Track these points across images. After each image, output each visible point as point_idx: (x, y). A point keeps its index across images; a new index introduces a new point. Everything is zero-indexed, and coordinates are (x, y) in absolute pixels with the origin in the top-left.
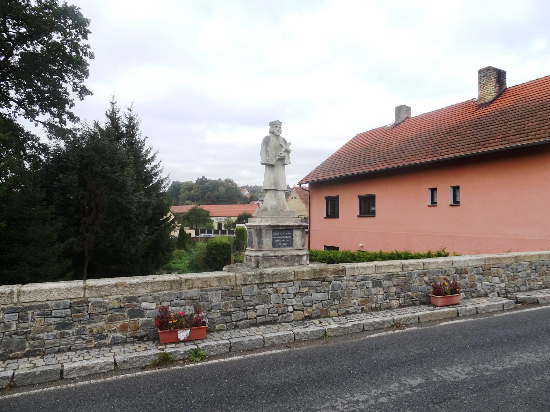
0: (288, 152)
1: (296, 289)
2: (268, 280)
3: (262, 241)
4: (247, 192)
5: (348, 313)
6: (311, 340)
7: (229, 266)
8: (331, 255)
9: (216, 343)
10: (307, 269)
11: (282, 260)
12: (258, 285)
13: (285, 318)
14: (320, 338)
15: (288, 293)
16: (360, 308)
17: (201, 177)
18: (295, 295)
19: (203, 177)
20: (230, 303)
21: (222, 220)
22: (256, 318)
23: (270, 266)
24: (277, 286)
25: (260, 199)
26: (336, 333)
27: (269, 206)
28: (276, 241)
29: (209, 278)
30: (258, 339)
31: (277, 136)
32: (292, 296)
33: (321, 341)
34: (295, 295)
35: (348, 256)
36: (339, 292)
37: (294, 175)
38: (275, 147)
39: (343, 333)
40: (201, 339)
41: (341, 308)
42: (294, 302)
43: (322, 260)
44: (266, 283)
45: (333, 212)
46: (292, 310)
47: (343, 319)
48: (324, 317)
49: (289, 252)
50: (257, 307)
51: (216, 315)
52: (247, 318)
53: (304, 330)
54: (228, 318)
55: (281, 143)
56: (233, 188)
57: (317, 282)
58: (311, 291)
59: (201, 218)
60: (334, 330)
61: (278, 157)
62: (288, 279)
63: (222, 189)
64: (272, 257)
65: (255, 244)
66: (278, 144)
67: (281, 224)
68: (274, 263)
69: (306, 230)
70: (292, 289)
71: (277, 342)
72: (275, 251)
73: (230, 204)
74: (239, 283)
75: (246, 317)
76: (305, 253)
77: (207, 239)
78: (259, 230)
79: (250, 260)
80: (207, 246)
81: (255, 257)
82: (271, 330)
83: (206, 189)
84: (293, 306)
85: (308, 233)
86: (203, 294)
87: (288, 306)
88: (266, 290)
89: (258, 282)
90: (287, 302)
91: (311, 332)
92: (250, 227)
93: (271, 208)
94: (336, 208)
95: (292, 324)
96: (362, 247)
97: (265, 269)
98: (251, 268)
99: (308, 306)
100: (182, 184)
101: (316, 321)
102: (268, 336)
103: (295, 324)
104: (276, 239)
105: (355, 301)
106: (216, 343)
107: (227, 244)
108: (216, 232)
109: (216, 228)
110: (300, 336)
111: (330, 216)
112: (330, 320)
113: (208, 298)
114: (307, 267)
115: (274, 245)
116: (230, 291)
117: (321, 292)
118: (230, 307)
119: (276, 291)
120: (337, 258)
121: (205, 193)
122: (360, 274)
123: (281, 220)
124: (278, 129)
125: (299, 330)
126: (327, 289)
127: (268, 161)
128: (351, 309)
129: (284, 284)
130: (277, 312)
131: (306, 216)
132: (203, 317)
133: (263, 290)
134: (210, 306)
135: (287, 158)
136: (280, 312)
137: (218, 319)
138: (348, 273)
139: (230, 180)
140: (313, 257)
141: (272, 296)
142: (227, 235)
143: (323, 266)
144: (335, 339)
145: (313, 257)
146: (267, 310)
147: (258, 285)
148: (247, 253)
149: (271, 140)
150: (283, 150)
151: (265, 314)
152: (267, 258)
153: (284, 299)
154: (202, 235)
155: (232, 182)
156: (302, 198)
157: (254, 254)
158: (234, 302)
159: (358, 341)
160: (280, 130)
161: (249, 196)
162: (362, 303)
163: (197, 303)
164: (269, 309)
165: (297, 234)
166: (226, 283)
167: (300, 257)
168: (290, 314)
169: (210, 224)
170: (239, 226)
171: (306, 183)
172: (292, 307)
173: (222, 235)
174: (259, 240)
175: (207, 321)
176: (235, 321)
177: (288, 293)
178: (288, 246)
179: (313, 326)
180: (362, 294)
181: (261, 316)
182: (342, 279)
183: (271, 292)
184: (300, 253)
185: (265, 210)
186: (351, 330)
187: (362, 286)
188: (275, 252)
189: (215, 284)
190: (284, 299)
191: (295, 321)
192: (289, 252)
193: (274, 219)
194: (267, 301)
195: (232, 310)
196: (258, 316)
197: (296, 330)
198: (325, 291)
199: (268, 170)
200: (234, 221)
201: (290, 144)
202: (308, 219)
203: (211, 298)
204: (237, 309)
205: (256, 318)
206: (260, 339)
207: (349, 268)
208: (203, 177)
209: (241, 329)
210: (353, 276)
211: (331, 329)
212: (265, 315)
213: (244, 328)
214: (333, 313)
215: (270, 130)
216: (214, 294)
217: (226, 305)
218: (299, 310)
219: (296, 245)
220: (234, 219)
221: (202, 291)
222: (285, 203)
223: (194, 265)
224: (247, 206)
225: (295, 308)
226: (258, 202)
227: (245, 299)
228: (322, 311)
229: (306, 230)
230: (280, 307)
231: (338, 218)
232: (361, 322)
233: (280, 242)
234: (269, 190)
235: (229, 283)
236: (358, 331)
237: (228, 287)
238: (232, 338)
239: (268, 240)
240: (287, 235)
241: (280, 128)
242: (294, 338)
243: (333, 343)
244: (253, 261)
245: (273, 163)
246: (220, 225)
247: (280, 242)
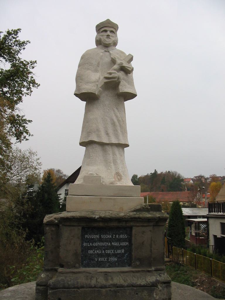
100: (183, 180)
135: (123, 83)
233: (101, 255)
240: (119, 240)
247: (101, 255)
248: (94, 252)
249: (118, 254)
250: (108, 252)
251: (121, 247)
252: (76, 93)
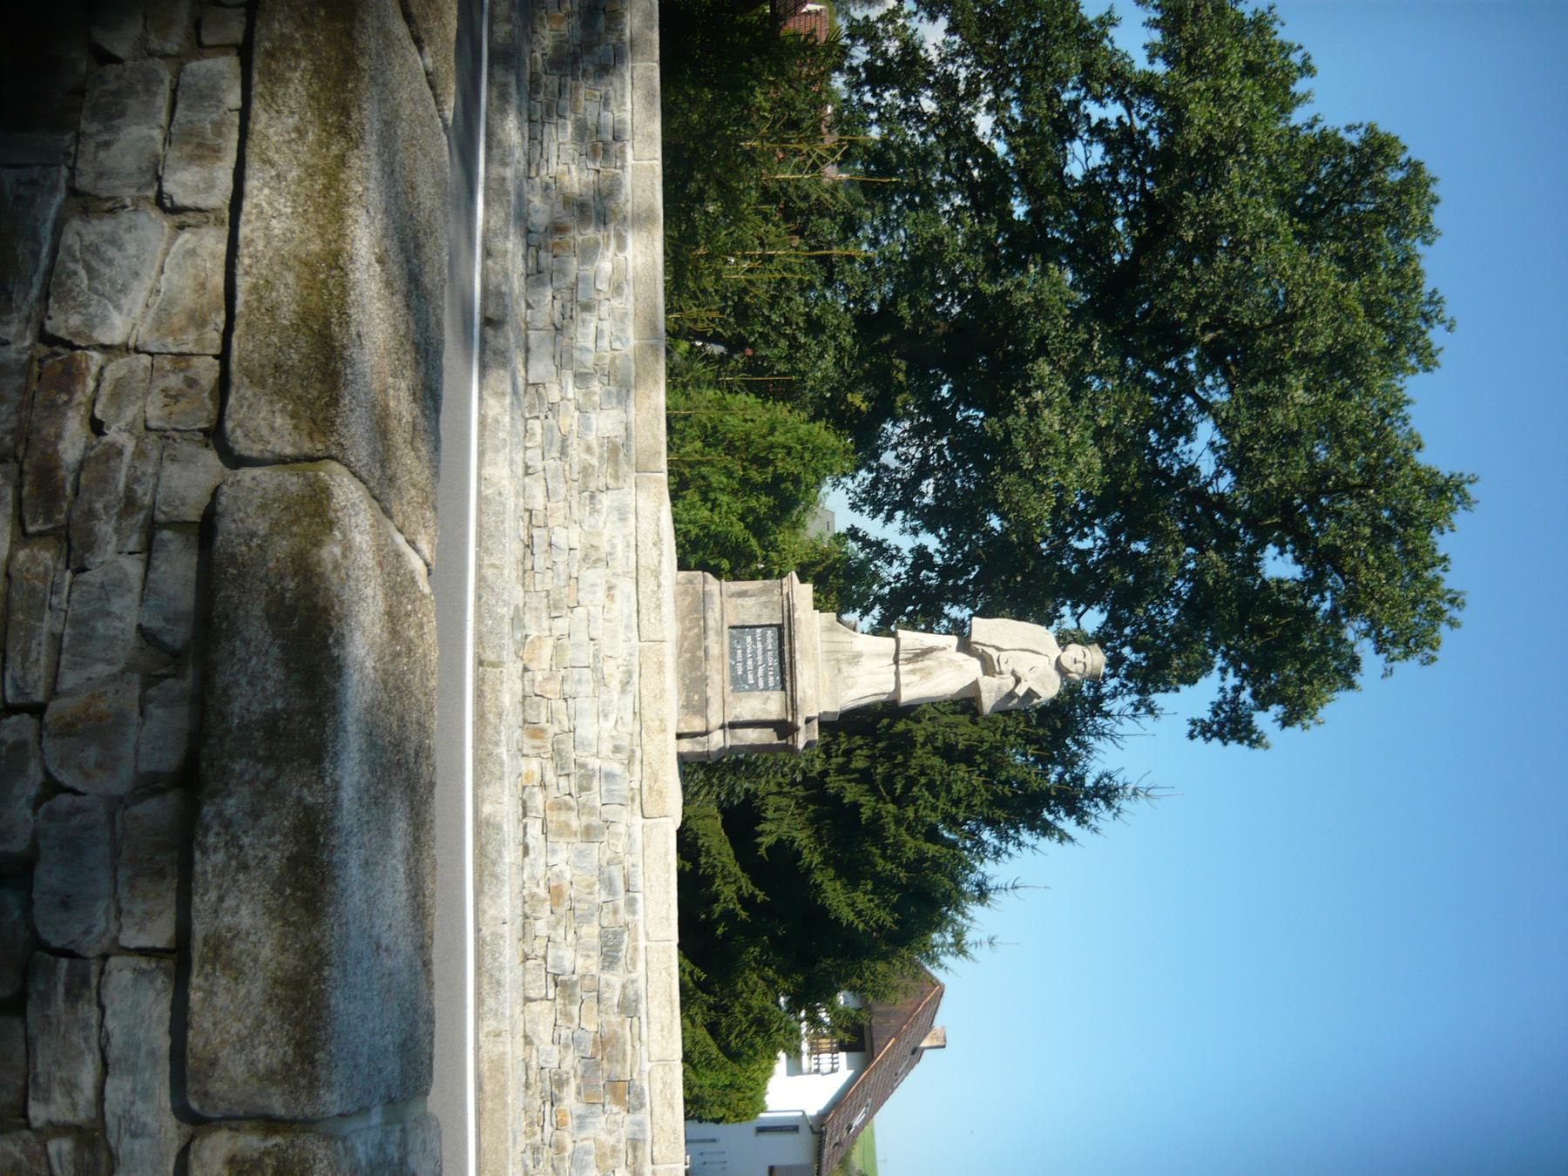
72: (720, 633)
233: (744, 653)
240: (765, 676)
247: (744, 653)
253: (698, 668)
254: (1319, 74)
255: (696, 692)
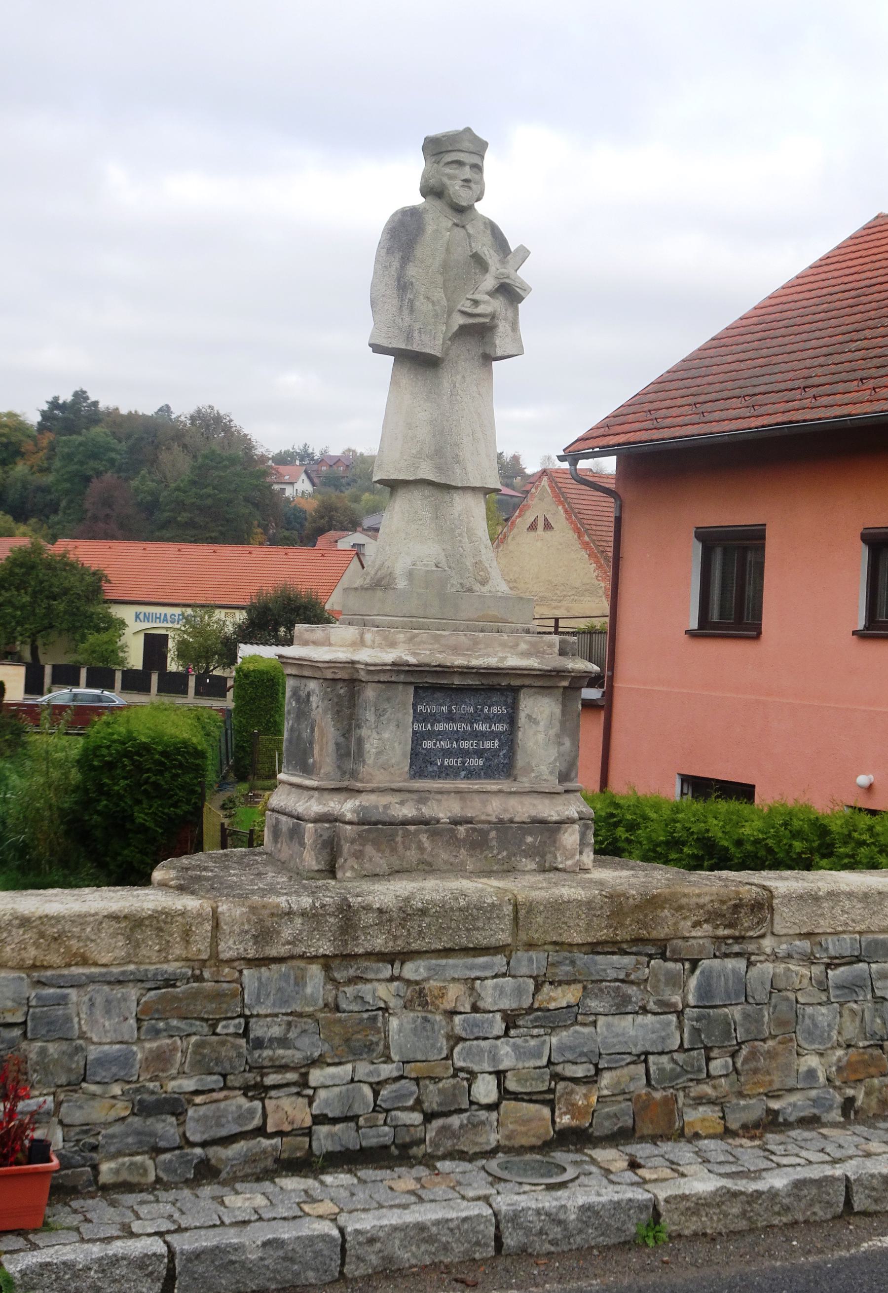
0: (510, 293)
1: (519, 992)
2: (379, 942)
3: (360, 742)
4: (303, 485)
5: (773, 1122)
6: (584, 1252)
7: (185, 860)
8: (716, 828)
9: (96, 1250)
10: (580, 894)
11: (453, 841)
12: (326, 962)
13: (454, 1135)
14: (626, 1245)
15: (475, 1009)
16: (839, 1099)
17: (66, 397)
18: (511, 1020)
19: (80, 396)
20: (182, 1048)
21: (169, 622)
22: (308, 1133)
23: (396, 872)
24: (423, 973)
25: (367, 522)
26: (709, 1223)
27: (400, 567)
28: (428, 744)
29: (80, 919)
30: (311, 1240)
31: (462, 210)
32: (499, 1027)
33: (634, 1259)
34: (511, 1020)
35: (796, 835)
36: (736, 1013)
37: (544, 408)
38: (445, 267)
39: (743, 1224)
40: (20, 1232)
41: (741, 1095)
42: (507, 1054)
43: (658, 853)
44: (368, 955)
45: (732, 607)
46: (493, 1097)
47: (748, 1152)
48: (654, 1139)
49: (494, 802)
50: (316, 1076)
51: (103, 1107)
52: (261, 1131)
53: (549, 1201)
54: (166, 1128)
55: (477, 247)
56: (233, 461)
57: (627, 960)
58: (594, 1004)
59: (60, 606)
60: (697, 1205)
61: (461, 320)
62: (481, 939)
63: (178, 465)
64: (405, 823)
65: (324, 753)
66: (460, 254)
67: (459, 661)
68: (412, 855)
69: (590, 686)
70: (502, 991)
71: (405, 1256)
72: (423, 797)
73: (213, 541)
74: (229, 948)
75: (257, 1122)
76: (572, 811)
77: (82, 715)
78: (347, 685)
79: (296, 834)
80: (85, 750)
81: (320, 819)
82: (381, 1194)
83: (94, 456)
84: (500, 1075)
85: (604, 708)
86: (43, 1002)
87: (472, 1076)
88: (365, 989)
89: (326, 948)
90: (468, 1054)
91: (585, 1209)
92: (307, 669)
93: (410, 575)
94: (749, 590)
95: (493, 1165)
96: (870, 788)
97: (366, 885)
98: (297, 875)
99: (575, 1080)
101: (611, 1157)
102: (366, 1222)
103: (504, 1167)
104: (429, 735)
105: (813, 1061)
106: (96, 1250)
107: (185, 743)
108: (135, 682)
109: (135, 659)
110: (528, 1231)
111: (716, 626)
112: (683, 1152)
113: (68, 1019)
114: (584, 885)
115: (421, 763)
116: (181, 988)
117: (644, 1010)
118: (181, 1073)
119: (419, 998)
120: (739, 843)
121: (87, 480)
122: (842, 927)
123: (462, 639)
124: (467, 173)
125: (524, 1199)
126: (677, 999)
127: (409, 338)
128: (790, 1105)
129: (456, 966)
130: (419, 1102)
131: (598, 623)
132: (36, 1118)
133: (350, 990)
134: (77, 1063)
135: (503, 327)
136: (432, 1103)
137: (117, 1129)
138: (786, 920)
139: (218, 419)
140: (621, 832)
141: (394, 1023)
142: (191, 699)
143: (659, 878)
144: (701, 1248)
145: (621, 832)
146: (367, 1091)
147: (326, 962)
148: (279, 799)
149: (430, 229)
150: (489, 282)
151: (358, 1109)
152: (377, 829)
153: (455, 1039)
154: (61, 695)
155: (227, 429)
156: (580, 526)
157: (313, 806)
158: (199, 1045)
159: (817, 1267)
160: (474, 182)
161: (311, 506)
162: (849, 1073)
163: (12, 1045)
164: (376, 1088)
165: (539, 715)
166: (165, 948)
167: (549, 829)
168: (483, 1115)
169: (104, 637)
170: (254, 659)
171: (605, 451)
172: (492, 1081)
173: (166, 699)
174: (346, 734)
175: (57, 1139)
176: (204, 1144)
177: (475, 1009)
178: (488, 772)
179: (596, 1181)
180: (851, 1030)
181: (334, 1121)
182: (751, 947)
183: (393, 1003)
184: (550, 810)
185: (381, 584)
186: (787, 1209)
187: (850, 988)
188: (423, 801)
189: (108, 951)
190: (455, 1039)
191: (508, 1150)
192: (494, 802)
193: (423, 635)
194: (370, 1047)
195: (189, 1084)
196: (319, 1119)
197: (506, 1200)
198: (666, 1008)
199: (405, 380)
200: (229, 629)
201: (524, 253)
202: (603, 642)
203: (81, 1022)
204: (214, 1081)
205: (308, 1133)
206: (325, 1238)
207: (788, 898)
208: (80, 396)
209: (231, 1182)
210: (809, 935)
211: (684, 1197)
212: (355, 1118)
213: (244, 1179)
214: (698, 1117)
215: (425, 178)
216: (99, 1000)
217: (161, 1059)
218: (530, 1098)
219: (528, 769)
220: (231, 620)
221: (40, 983)
222: (487, 553)
223: (13, 845)
224: (298, 555)
225: (512, 1085)
226: (357, 537)
227: (258, 1030)
228: (642, 1107)
229: (592, 694)
230: (436, 1080)
231: (758, 636)
232: (838, 1171)
233: (447, 753)
234: (405, 483)
235: (178, 950)
236: (820, 1213)
237: (172, 967)
238: (180, 1230)
239: (387, 739)
240: (488, 719)
241: (478, 168)
242: (498, 1238)
243: (692, 1273)
244: (308, 840)
245: (433, 347)
246: (155, 645)
247: (447, 753)
248: (435, 744)
249: (486, 750)
250: (465, 745)
251: (492, 735)
252: (373, 342)
253: (484, 834)
254: (860, 530)
255: (522, 841)
